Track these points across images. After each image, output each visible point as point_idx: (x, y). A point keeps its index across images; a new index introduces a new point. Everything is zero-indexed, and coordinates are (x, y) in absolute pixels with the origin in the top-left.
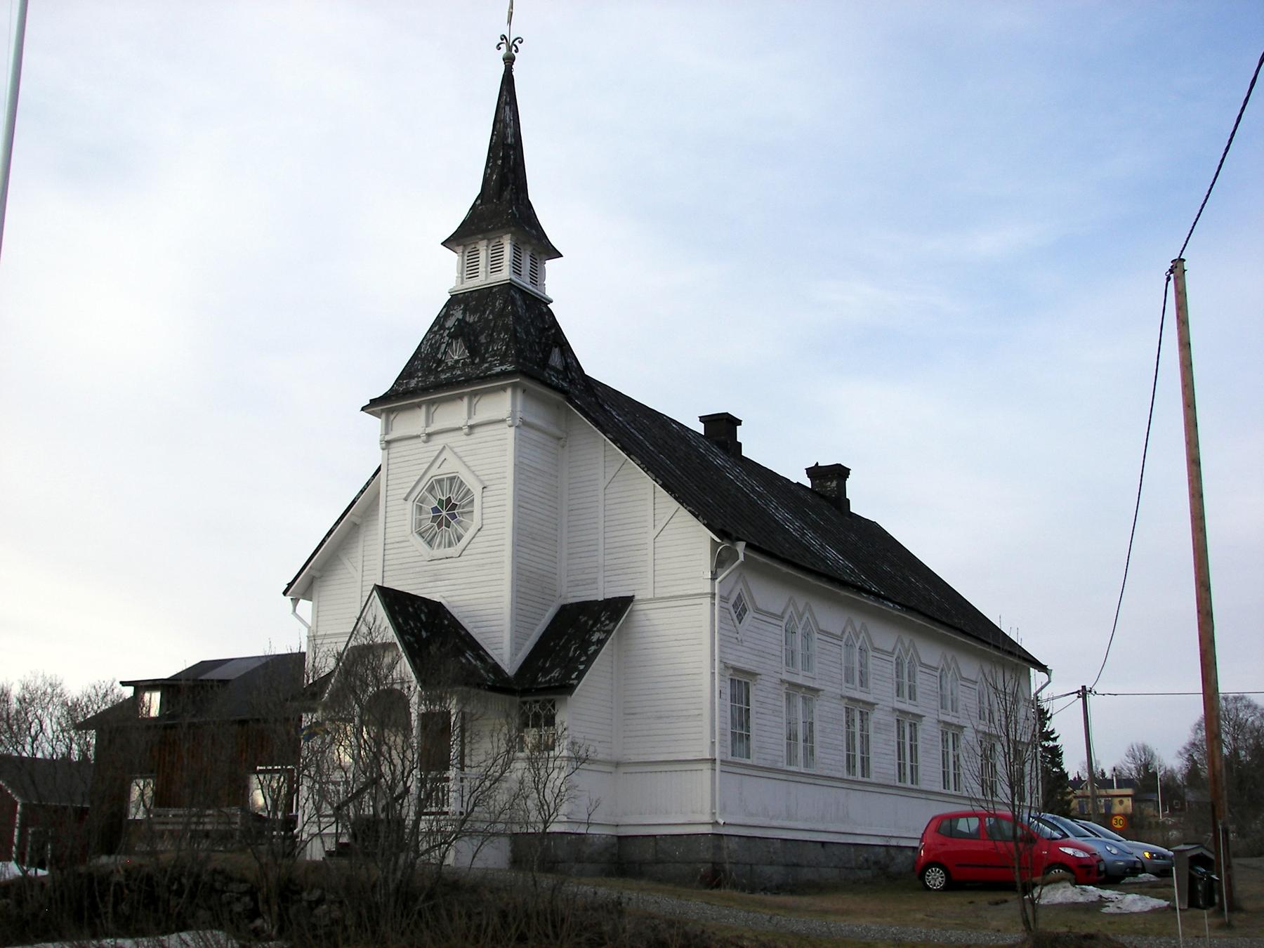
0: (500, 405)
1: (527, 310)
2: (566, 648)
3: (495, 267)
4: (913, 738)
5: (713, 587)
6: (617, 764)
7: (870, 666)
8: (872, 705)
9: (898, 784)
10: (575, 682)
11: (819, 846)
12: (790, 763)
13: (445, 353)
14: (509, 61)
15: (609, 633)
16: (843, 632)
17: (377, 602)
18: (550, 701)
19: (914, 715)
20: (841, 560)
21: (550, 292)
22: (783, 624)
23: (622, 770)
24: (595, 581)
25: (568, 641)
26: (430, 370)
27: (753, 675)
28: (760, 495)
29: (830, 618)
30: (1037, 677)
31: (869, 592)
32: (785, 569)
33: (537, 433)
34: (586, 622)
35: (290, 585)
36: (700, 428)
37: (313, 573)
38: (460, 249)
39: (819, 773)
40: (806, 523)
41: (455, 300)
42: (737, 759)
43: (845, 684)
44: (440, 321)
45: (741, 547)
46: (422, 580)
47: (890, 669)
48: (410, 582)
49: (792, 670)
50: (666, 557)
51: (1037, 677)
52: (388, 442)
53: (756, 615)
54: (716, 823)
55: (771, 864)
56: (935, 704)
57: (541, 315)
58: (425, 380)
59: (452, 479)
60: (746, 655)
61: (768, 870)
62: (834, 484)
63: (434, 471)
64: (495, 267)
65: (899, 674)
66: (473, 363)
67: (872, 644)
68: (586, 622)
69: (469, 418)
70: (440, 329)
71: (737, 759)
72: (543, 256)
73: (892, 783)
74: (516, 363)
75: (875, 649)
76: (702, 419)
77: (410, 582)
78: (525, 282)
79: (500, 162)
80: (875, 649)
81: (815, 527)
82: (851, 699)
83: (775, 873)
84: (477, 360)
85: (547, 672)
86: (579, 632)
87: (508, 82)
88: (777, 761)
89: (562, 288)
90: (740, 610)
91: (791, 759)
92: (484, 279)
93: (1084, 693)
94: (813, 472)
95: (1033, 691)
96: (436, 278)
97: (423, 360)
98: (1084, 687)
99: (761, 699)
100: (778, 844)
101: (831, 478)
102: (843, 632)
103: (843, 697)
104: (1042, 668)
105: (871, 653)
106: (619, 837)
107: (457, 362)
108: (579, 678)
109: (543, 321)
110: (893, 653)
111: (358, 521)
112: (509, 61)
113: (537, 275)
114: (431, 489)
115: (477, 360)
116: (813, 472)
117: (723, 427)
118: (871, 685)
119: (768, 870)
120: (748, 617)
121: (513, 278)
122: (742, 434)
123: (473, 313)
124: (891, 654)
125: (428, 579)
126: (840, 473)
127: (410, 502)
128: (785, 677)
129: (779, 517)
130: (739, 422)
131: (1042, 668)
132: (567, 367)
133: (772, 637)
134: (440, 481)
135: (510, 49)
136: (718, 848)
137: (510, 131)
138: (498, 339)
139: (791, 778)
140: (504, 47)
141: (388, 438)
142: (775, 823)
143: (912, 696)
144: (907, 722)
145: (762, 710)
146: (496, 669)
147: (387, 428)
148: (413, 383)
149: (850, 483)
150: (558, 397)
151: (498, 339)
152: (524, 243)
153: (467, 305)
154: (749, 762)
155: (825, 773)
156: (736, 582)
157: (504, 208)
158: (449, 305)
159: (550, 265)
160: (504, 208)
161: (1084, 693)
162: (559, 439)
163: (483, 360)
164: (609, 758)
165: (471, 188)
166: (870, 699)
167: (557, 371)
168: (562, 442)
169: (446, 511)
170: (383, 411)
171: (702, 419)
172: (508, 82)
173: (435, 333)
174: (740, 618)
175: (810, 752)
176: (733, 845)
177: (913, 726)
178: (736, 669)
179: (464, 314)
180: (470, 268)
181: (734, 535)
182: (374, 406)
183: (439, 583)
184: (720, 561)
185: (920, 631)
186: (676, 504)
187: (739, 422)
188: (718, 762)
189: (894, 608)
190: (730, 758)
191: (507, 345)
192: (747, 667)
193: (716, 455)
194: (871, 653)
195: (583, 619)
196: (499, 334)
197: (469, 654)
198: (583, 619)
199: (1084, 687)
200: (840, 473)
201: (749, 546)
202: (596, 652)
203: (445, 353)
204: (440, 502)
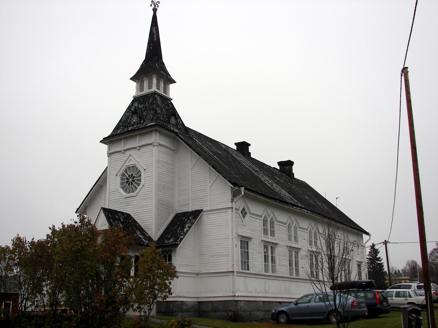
0: (155, 138)
1: (162, 102)
2: (176, 230)
3: (150, 87)
4: (296, 257)
5: (232, 205)
6: (198, 274)
7: (299, 235)
8: (299, 249)
9: (289, 276)
10: (179, 243)
11: (279, 303)
12: (290, 275)
13: (131, 119)
14: (155, 10)
15: (192, 224)
16: (287, 221)
17: (102, 214)
18: (170, 250)
19: (273, 243)
20: (287, 194)
21: (171, 96)
22: (262, 219)
23: (199, 276)
24: (188, 204)
25: (178, 227)
26: (125, 126)
27: (250, 238)
28: (256, 171)
29: (282, 217)
30: (365, 237)
31: (297, 206)
32: (262, 198)
33: (166, 149)
34: (185, 220)
35: (78, 209)
36: (235, 147)
37: (86, 204)
38: (137, 81)
39: (279, 275)
40: (274, 181)
41: (136, 99)
42: (244, 271)
43: (288, 241)
44: (129, 108)
45: (243, 189)
46: (123, 205)
47: (306, 235)
48: (118, 206)
49: (266, 236)
50: (209, 192)
51: (365, 237)
52: (110, 154)
53: (250, 215)
54: (235, 296)
55: (258, 311)
56: (286, 237)
57: (168, 105)
58: (125, 131)
59: (133, 167)
60: (247, 231)
61: (258, 313)
62: (288, 167)
63: (127, 164)
64: (150, 87)
65: (310, 237)
66: (140, 123)
67: (299, 226)
68: (185, 220)
69: (139, 143)
70: (129, 111)
71: (244, 271)
72: (169, 82)
73: (261, 273)
74: (156, 122)
75: (301, 228)
76: (236, 144)
77: (118, 206)
78: (161, 92)
79: (151, 48)
80: (301, 228)
81: (278, 183)
82: (290, 247)
83: (261, 314)
84: (142, 121)
85: (169, 239)
86: (183, 223)
87: (155, 19)
88: (260, 271)
89: (177, 95)
90: (244, 213)
91: (266, 270)
92: (146, 91)
93: (385, 243)
94: (280, 163)
95: (364, 242)
96: (129, 92)
97: (123, 122)
98: (385, 241)
99: (253, 247)
100: (261, 303)
101: (287, 166)
102: (287, 221)
103: (287, 246)
104: (367, 234)
105: (299, 229)
106: (199, 302)
107: (135, 122)
108: (180, 241)
109: (169, 107)
110: (308, 229)
111: (102, 184)
112: (155, 10)
113: (166, 90)
114: (126, 171)
115: (142, 121)
116: (280, 163)
117: (243, 147)
118: (299, 241)
119: (258, 313)
120: (247, 216)
121: (156, 90)
122: (251, 149)
123: (141, 104)
124: (307, 229)
125: (125, 205)
126: (290, 164)
127: (118, 176)
128: (263, 239)
129: (263, 179)
130: (250, 145)
131: (367, 234)
132: (177, 123)
133: (258, 224)
134: (129, 168)
135: (155, 6)
136: (236, 305)
137: (155, 36)
138: (151, 114)
139: (266, 278)
140: (153, 5)
141: (110, 152)
142: (260, 295)
143: (296, 239)
144: (294, 251)
145: (254, 252)
146: (150, 239)
147: (109, 149)
148: (119, 131)
149: (294, 167)
150: (174, 135)
151: (151, 114)
152: (161, 78)
153: (139, 101)
154: (248, 272)
155: (281, 275)
156: (242, 203)
157: (153, 65)
158: (133, 102)
159: (172, 86)
160: (153, 65)
161: (385, 243)
162: (174, 150)
163: (144, 121)
164: (194, 272)
165: (142, 57)
166: (299, 247)
167: (173, 125)
168: (175, 152)
169: (131, 179)
170: (108, 142)
171: (236, 144)
172: (155, 19)
173: (128, 112)
174: (244, 217)
175: (297, 270)
176: (242, 304)
177: (297, 254)
178: (242, 237)
179: (138, 105)
180: (141, 88)
181: (240, 185)
182: (105, 141)
183: (129, 206)
184: (235, 194)
185: (348, 231)
186: (427, 244)
187: (250, 145)
188: (235, 272)
189: (307, 212)
190: (241, 271)
191: (153, 115)
192: (247, 235)
193: (240, 157)
194: (299, 229)
195: (183, 219)
196: (150, 111)
197: (138, 233)
198: (183, 219)
199: (385, 241)
200: (290, 164)
201: (246, 189)
202: (187, 231)
203: (131, 119)
204: (129, 175)
